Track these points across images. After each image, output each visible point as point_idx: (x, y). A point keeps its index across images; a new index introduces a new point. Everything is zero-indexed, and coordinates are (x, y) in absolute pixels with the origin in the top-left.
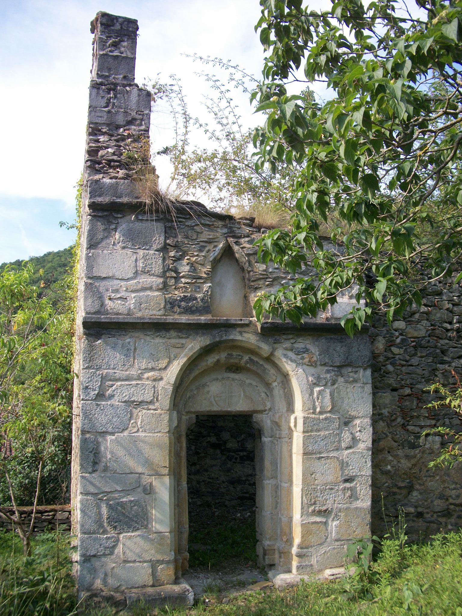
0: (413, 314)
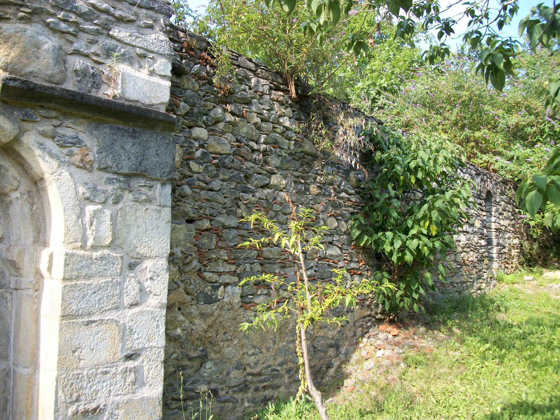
0: (218, 122)
